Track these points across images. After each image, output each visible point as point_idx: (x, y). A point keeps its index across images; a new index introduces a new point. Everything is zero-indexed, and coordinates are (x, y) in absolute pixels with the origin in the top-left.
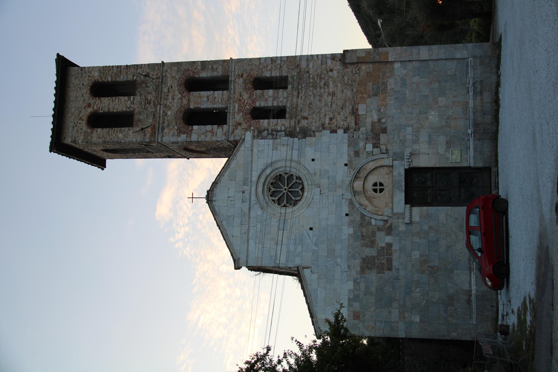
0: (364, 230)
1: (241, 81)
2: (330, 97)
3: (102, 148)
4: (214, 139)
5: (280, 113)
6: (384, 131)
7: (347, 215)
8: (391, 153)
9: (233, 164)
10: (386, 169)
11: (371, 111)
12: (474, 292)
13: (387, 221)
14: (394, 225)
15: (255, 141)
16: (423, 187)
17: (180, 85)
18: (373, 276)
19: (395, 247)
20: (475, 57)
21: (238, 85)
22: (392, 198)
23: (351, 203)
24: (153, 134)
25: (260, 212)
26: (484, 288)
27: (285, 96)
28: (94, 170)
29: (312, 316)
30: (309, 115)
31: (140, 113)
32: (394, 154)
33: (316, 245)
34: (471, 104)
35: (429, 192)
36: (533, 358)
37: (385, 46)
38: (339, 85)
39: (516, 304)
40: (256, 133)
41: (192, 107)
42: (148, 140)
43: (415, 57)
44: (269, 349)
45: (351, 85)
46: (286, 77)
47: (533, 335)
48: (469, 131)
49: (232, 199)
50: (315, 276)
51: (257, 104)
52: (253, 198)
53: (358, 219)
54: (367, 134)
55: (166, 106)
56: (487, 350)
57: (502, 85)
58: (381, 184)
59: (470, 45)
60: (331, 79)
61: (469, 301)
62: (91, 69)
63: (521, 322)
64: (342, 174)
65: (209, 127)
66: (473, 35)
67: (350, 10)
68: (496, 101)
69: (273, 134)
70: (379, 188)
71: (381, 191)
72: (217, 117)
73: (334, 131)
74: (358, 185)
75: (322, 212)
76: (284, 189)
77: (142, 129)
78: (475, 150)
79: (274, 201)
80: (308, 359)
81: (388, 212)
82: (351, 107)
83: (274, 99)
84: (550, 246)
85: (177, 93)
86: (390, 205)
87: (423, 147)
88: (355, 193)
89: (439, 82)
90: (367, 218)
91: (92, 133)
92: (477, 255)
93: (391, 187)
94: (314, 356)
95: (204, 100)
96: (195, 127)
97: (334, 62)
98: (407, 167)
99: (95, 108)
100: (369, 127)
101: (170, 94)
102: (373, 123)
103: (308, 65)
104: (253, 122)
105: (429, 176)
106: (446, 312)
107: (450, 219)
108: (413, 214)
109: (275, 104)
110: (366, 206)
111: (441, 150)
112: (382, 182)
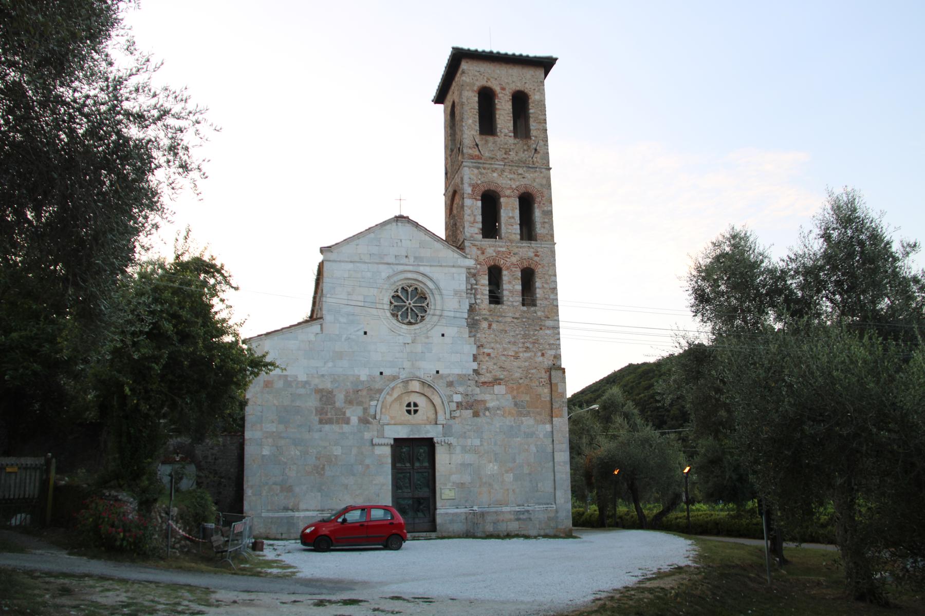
0: (364, 393)
1: (531, 254)
2: (513, 354)
3: (456, 101)
4: (467, 225)
5: (495, 298)
6: (476, 414)
7: (381, 373)
8: (452, 422)
9: (438, 245)
10: (433, 416)
11: (497, 399)
12: (297, 514)
13: (375, 418)
14: (371, 426)
15: (464, 270)
16: (414, 460)
17: (526, 187)
18: (313, 403)
19: (346, 428)
20: (557, 511)
21: (526, 251)
22: (400, 424)
23: (394, 378)
24: (472, 157)
25: (384, 275)
26: (302, 527)
27: (515, 304)
28: (433, 92)
29: (268, 334)
30: (494, 330)
31: (494, 142)
32: (450, 426)
33: (348, 339)
34: (505, 509)
35: (408, 465)
36: (235, 574)
37: (569, 413)
38: (527, 364)
39: (287, 559)
40: (473, 271)
41: (502, 200)
42: (465, 151)
43: (557, 447)
44: (236, 289)
45: (526, 377)
46: (535, 305)
47: (258, 574)
48: (475, 508)
49: (399, 244)
50: (312, 338)
51: (505, 273)
52: (401, 268)
53: (377, 386)
54: (473, 395)
55: (503, 171)
56: (238, 526)
57: (526, 541)
58: (416, 411)
59: (569, 506)
60: (533, 354)
61: (286, 509)
62: (542, 92)
63: (269, 563)
64: (427, 368)
65: (479, 218)
66: (581, 509)
67: (609, 373)
68: (508, 536)
69: (472, 290)
70: (412, 409)
71: (409, 412)
72: (490, 228)
73: (475, 358)
74: (415, 386)
75: (386, 346)
76: (410, 303)
77: (477, 145)
78: (456, 514)
79: (397, 291)
80: (223, 332)
81: (385, 419)
82: (502, 377)
83: (511, 292)
84: (354, 592)
85: (518, 183)
86: (393, 422)
87: (458, 457)
88: (406, 382)
89: (530, 474)
90: (378, 396)
91: (473, 91)
92: (339, 517)
93: (413, 422)
94: (228, 339)
95: (509, 213)
96: (479, 203)
97: (552, 358)
98: (435, 440)
99: (500, 95)
100: (480, 398)
101: (516, 176)
102: (484, 402)
103: (548, 328)
104: (486, 268)
105: (426, 464)
106: (274, 484)
107: (376, 489)
108: (382, 448)
109: (505, 293)
110: (391, 395)
111: (455, 478)
112: (419, 413)
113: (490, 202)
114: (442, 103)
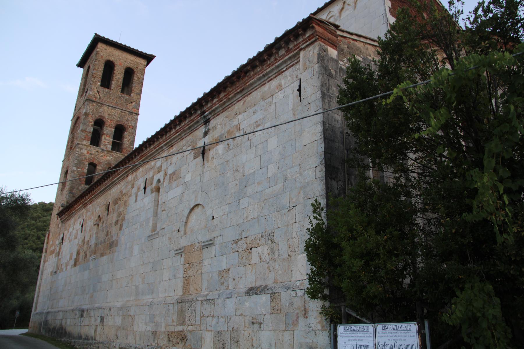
28: (78, 60)
72: (95, 140)
113: (99, 123)
114: (82, 67)
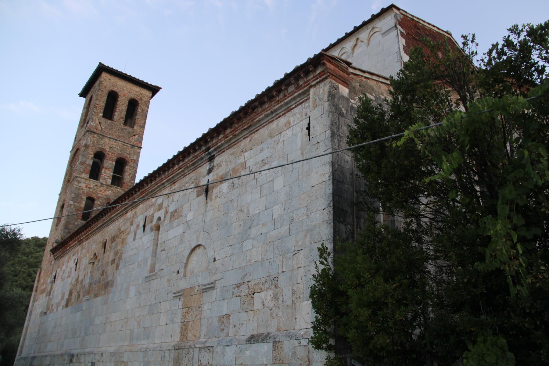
28: (80, 89)
96: (114, 163)
113: (100, 156)
114: (85, 97)
